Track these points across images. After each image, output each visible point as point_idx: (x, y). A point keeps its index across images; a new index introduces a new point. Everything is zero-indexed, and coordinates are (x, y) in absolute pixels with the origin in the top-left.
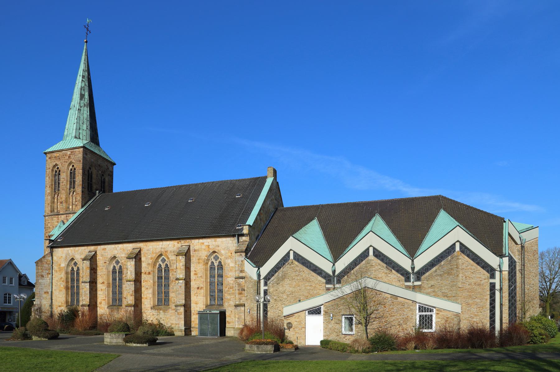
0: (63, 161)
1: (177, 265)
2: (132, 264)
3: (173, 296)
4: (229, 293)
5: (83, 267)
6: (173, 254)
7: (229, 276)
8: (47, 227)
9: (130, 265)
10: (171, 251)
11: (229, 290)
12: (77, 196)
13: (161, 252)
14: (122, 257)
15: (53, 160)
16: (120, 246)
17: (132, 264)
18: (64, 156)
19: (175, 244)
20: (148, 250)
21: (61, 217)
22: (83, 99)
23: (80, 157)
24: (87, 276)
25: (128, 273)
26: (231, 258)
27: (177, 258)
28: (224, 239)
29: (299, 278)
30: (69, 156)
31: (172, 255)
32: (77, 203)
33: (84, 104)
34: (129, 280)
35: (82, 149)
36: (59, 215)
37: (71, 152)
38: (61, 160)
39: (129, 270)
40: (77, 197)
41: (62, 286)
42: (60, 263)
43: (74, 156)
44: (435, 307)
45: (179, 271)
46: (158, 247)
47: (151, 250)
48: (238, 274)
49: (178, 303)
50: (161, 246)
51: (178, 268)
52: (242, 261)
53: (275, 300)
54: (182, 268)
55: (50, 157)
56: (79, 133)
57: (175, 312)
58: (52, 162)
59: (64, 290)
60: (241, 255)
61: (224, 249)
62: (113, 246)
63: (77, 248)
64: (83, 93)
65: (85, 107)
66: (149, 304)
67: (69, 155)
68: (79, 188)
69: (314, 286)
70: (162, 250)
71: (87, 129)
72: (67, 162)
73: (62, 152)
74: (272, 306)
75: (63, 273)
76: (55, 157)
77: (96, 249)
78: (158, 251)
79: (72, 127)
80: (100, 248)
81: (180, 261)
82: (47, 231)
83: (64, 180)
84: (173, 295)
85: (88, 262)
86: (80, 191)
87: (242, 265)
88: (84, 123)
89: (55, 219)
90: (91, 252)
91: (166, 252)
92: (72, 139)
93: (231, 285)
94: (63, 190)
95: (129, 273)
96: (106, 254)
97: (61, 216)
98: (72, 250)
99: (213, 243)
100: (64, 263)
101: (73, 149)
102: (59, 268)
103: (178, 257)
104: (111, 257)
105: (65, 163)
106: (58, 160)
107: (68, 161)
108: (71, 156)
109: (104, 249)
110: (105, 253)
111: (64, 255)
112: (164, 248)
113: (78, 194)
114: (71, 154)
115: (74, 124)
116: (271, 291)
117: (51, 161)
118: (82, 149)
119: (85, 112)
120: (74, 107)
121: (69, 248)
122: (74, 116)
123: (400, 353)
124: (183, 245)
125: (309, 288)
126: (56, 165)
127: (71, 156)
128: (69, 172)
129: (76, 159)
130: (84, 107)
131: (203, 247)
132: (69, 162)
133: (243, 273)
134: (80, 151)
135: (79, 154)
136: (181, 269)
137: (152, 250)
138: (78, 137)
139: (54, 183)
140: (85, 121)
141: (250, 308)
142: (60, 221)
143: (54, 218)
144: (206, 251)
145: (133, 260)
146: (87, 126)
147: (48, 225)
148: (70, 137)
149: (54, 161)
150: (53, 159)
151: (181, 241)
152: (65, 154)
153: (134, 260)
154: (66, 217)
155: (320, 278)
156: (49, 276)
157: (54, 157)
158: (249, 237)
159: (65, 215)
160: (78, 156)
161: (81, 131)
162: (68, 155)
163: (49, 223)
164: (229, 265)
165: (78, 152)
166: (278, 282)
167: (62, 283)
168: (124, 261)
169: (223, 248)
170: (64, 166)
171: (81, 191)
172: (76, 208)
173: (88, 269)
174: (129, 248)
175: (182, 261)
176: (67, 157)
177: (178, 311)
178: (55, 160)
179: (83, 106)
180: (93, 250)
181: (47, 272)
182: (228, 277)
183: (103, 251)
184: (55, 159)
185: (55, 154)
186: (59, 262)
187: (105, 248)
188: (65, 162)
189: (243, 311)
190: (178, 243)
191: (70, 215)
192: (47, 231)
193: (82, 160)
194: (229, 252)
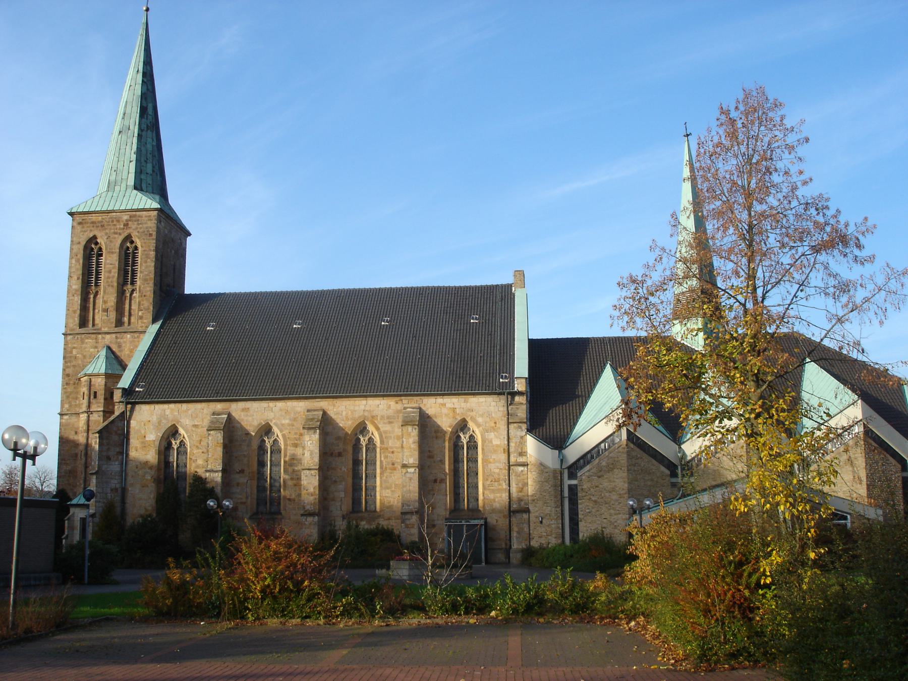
0: (113, 231)
1: (403, 442)
2: (314, 439)
3: (387, 495)
4: (493, 490)
5: (208, 444)
6: (386, 421)
7: (491, 460)
8: (71, 357)
9: (310, 440)
10: (382, 417)
11: (492, 484)
12: (143, 301)
13: (365, 416)
14: (283, 425)
15: (89, 227)
16: (280, 404)
17: (314, 439)
18: (115, 223)
19: (390, 405)
20: (337, 414)
21: (103, 338)
22: (145, 116)
23: (151, 228)
24: (216, 459)
25: (306, 455)
26: (494, 430)
27: (402, 430)
28: (482, 399)
29: (636, 469)
30: (125, 222)
31: (384, 423)
32: (143, 314)
33: (147, 125)
34: (307, 468)
35: (155, 213)
36: (100, 333)
37: (130, 217)
38: (105, 229)
39: (307, 449)
40: (142, 303)
41: (149, 478)
42: (145, 432)
43: (138, 224)
44: (849, 514)
45: (407, 452)
46: (357, 408)
47: (344, 413)
48: (515, 459)
49: (407, 508)
50: (362, 407)
51: (404, 445)
52: (522, 437)
53: (595, 502)
54: (412, 446)
55: (81, 221)
56: (141, 179)
57: (402, 523)
58: (85, 232)
59: (153, 484)
60: (520, 427)
61: (482, 416)
62: (264, 404)
63: (185, 406)
64: (145, 105)
65: (149, 131)
66: (339, 509)
67: (127, 220)
68: (146, 285)
69: (655, 480)
70: (366, 414)
71: (153, 171)
72: (120, 234)
73: (110, 214)
74: (589, 512)
75: (151, 453)
76: (93, 223)
77: (228, 409)
78: (357, 416)
79: (126, 167)
80: (235, 407)
81: (409, 435)
82: (69, 364)
83: (113, 268)
84: (388, 493)
85: (219, 434)
86: (150, 290)
87: (522, 444)
88: (148, 161)
89: (90, 341)
90: (219, 414)
91: (373, 417)
92: (129, 190)
93: (496, 476)
94: (109, 286)
95: (307, 454)
96: (250, 419)
97: (104, 336)
98: (172, 410)
99: (462, 404)
100: (154, 433)
101: (136, 211)
102: (143, 443)
103: (405, 428)
104: (259, 424)
105: (116, 236)
106: (100, 228)
107: (124, 232)
108: (130, 223)
109: (246, 410)
110: (247, 415)
111: (154, 419)
112: (369, 411)
113: (145, 296)
114: (130, 221)
115: (130, 162)
116: (585, 487)
117: (84, 230)
118: (155, 213)
119: (150, 140)
120: (129, 129)
121: (166, 406)
122: (128, 148)
123: (116, 609)
124: (405, 406)
125: (649, 483)
126: (95, 237)
127: (130, 223)
128: (123, 253)
129: (141, 230)
130: (147, 131)
131: (444, 411)
132: (126, 234)
133: (524, 457)
134: (150, 216)
135: (149, 222)
136: (411, 448)
137: (346, 414)
138: (138, 187)
139: (86, 272)
140: (150, 156)
141: (542, 515)
142: (100, 345)
143: (87, 338)
144: (450, 418)
145: (315, 432)
146: (153, 167)
147: (71, 352)
148: (124, 185)
149: (91, 230)
150: (88, 225)
151: (402, 400)
152: (115, 218)
153: (318, 431)
154: (117, 338)
155: (663, 469)
156: (120, 457)
157: (90, 221)
158: (525, 397)
159: (114, 336)
160: (146, 225)
161: (143, 177)
162: (123, 222)
163: (74, 348)
164: (491, 442)
165: (146, 217)
166: (600, 474)
167: (149, 471)
168: (287, 431)
169: (481, 413)
170: (113, 240)
171: (153, 291)
172: (140, 323)
173: (220, 446)
174: (299, 409)
175: (413, 434)
176: (120, 225)
177: (408, 522)
178: (92, 228)
179: (145, 129)
180: (221, 411)
181: (118, 450)
182: (490, 463)
183: (242, 413)
184: (93, 227)
185: (94, 218)
186: (143, 432)
187: (248, 408)
188: (115, 233)
189: (527, 521)
190: (397, 403)
191: (125, 335)
192: (69, 364)
193: (154, 233)
194: (491, 421)
